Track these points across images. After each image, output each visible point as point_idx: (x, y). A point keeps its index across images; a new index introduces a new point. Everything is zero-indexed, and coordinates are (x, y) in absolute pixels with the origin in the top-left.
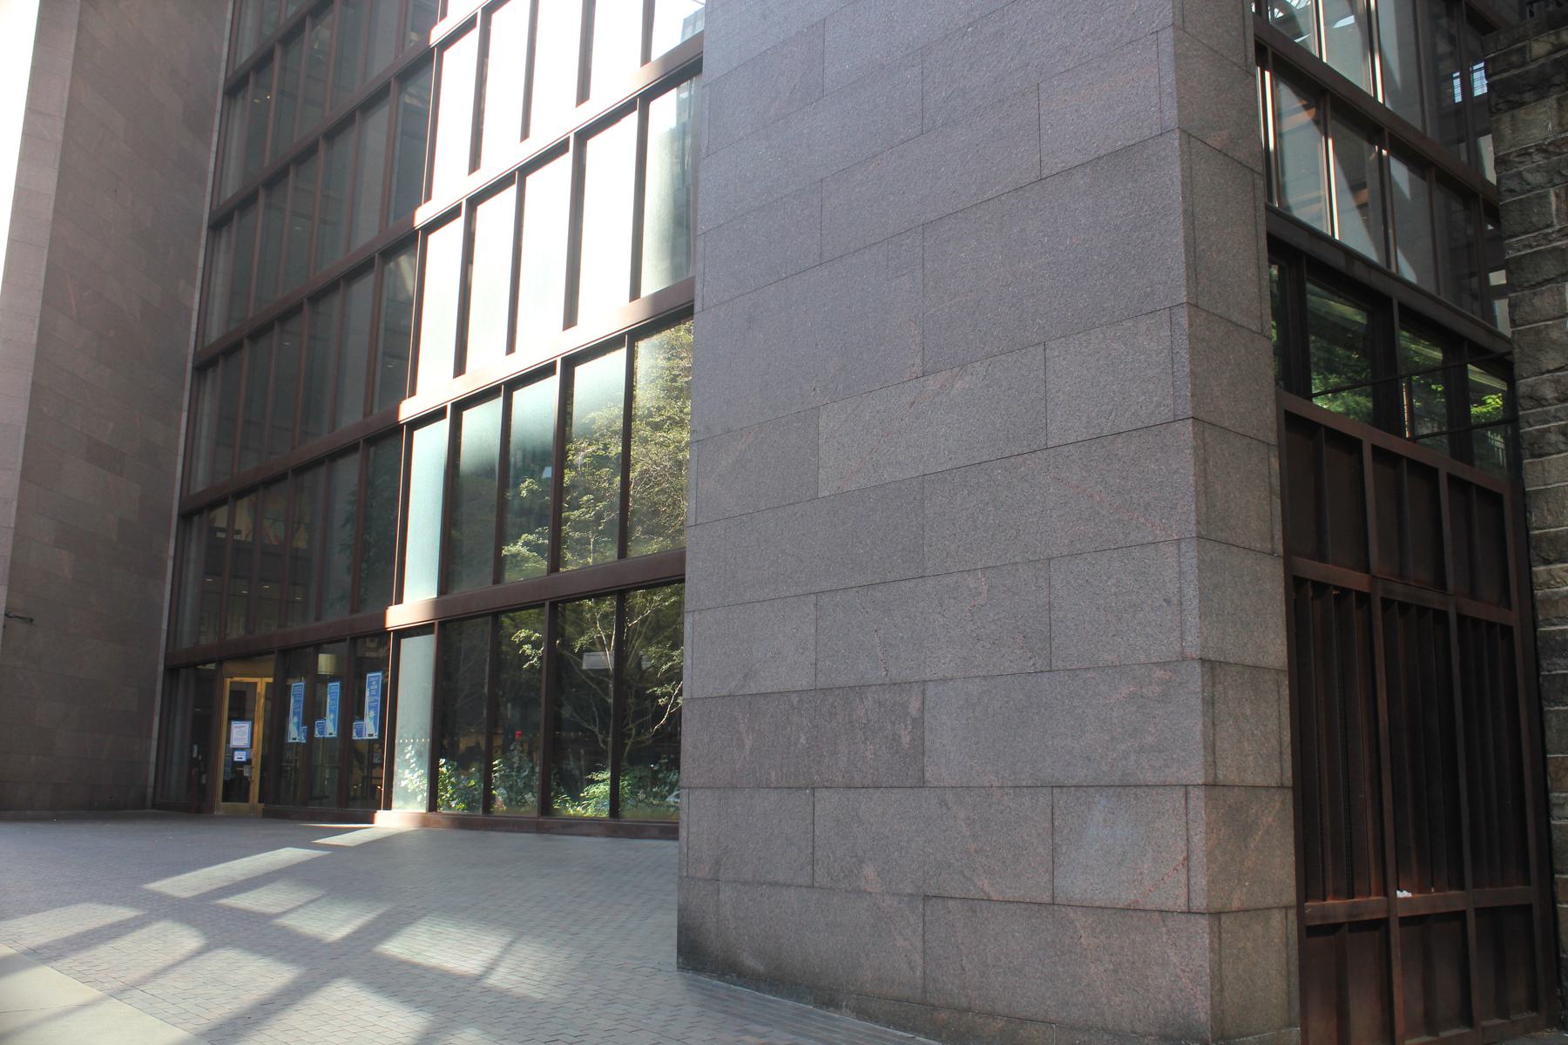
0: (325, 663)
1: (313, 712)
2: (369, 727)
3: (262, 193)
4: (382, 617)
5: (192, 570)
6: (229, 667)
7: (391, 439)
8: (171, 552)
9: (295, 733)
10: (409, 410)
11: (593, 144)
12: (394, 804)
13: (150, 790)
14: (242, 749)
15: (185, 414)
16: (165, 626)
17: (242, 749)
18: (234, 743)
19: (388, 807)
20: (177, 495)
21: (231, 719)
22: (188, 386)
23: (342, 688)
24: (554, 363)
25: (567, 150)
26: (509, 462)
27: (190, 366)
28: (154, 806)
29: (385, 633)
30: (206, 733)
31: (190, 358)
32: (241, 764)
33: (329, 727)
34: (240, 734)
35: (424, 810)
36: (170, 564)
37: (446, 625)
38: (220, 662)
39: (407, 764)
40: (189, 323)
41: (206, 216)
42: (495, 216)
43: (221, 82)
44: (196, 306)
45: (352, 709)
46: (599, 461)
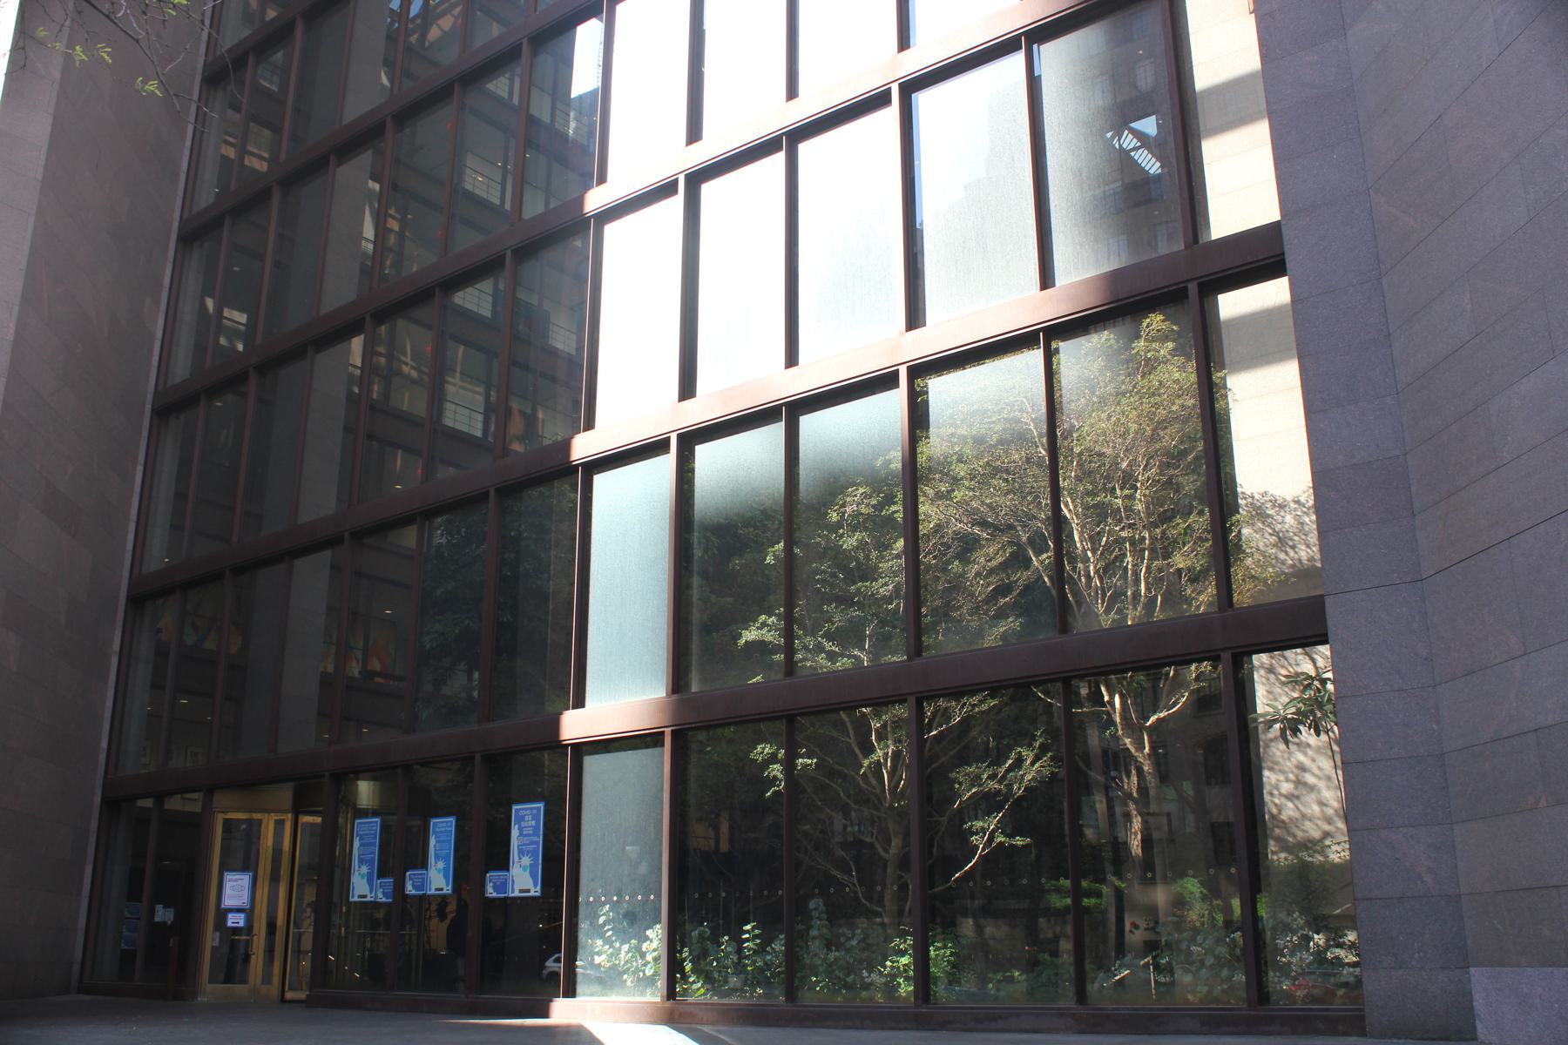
0: (365, 791)
1: (402, 854)
2: (522, 878)
3: (277, 193)
4: (555, 725)
5: (141, 675)
6: (220, 799)
7: (555, 488)
8: (116, 646)
9: (363, 886)
10: (584, 447)
11: (708, 190)
12: (580, 989)
13: (76, 968)
14: (239, 910)
15: (140, 469)
16: (104, 744)
17: (239, 910)
18: (229, 901)
19: (571, 992)
20: (126, 574)
21: (225, 867)
22: (145, 433)
23: (459, 828)
24: (896, 374)
25: (675, 192)
26: (796, 507)
27: (148, 407)
28: (82, 989)
29: (557, 746)
30: (187, 889)
31: (150, 397)
32: (236, 931)
33: (437, 878)
34: (236, 890)
35: (658, 999)
36: (115, 661)
37: (694, 735)
38: (210, 792)
39: (598, 931)
40: (151, 351)
41: (176, 225)
42: (743, 207)
43: (200, 66)
44: (159, 335)
45: (484, 849)
46: (877, 524)
